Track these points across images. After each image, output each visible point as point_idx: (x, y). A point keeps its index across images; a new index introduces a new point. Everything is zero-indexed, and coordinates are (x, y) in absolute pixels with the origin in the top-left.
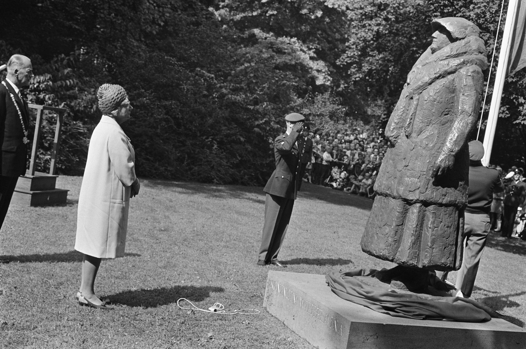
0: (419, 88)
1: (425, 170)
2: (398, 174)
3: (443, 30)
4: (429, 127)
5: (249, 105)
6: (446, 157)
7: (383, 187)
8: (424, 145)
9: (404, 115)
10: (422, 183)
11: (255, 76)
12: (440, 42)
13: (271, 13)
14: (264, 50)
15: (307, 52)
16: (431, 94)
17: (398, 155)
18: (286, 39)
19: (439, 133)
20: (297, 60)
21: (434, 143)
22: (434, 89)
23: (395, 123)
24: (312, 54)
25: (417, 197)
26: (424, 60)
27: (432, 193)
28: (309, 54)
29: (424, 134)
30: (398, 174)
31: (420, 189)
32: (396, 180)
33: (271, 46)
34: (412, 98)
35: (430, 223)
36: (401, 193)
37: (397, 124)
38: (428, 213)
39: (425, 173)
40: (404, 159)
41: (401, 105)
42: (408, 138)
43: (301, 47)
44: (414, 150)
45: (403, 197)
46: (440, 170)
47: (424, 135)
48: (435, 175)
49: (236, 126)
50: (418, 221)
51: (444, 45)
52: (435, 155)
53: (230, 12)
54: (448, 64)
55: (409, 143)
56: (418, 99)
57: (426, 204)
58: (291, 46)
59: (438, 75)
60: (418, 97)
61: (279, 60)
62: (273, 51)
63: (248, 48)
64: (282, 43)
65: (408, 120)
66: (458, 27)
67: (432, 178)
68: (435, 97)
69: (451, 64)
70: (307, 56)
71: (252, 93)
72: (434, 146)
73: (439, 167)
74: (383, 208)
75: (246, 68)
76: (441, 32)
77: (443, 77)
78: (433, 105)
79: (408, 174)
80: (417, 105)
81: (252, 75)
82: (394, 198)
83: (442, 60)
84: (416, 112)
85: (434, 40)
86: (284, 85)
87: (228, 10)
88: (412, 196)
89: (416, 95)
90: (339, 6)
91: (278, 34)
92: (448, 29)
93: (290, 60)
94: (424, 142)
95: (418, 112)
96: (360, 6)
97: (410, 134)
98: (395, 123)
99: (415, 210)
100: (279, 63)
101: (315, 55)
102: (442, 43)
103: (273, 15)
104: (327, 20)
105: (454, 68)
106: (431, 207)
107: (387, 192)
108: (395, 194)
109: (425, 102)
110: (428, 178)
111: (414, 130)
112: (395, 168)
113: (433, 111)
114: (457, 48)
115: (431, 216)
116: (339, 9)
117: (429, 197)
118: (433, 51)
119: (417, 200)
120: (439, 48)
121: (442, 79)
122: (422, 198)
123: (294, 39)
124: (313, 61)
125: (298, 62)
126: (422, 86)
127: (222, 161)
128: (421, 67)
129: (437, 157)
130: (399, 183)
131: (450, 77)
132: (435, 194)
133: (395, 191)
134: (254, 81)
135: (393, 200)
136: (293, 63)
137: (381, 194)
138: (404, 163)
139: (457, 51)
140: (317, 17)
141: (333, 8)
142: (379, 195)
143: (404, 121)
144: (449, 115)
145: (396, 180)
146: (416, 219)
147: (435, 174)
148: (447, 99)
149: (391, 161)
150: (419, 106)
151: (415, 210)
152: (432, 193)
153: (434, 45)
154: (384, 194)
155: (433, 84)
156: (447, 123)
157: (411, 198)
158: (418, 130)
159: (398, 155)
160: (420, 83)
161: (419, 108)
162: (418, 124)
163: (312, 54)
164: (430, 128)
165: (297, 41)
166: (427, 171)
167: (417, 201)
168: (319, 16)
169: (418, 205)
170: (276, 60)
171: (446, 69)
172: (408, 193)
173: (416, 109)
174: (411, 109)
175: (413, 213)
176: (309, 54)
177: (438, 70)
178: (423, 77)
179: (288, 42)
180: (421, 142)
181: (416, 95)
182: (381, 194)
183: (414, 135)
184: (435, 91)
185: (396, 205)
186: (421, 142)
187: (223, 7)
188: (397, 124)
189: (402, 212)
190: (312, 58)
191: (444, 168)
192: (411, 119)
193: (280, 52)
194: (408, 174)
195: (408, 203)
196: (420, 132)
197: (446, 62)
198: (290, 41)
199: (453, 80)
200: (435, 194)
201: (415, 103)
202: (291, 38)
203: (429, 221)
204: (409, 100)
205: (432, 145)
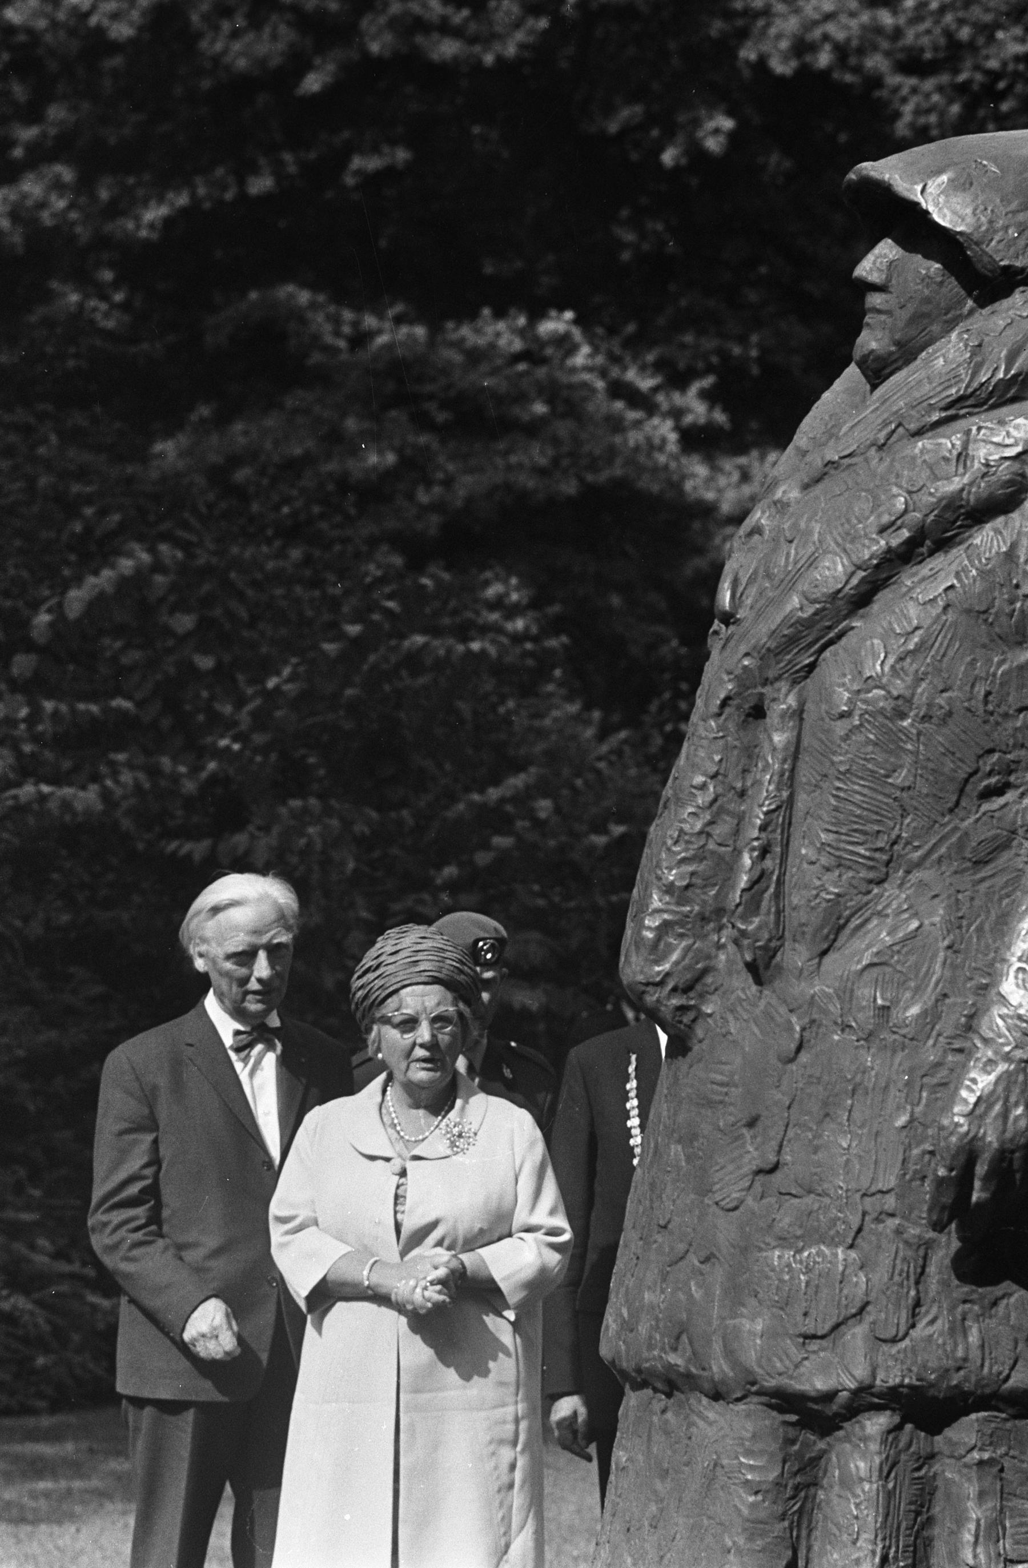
0: (792, 641)
1: (892, 1182)
2: (725, 1231)
3: (913, 227)
4: (890, 889)
5: (170, 834)
6: (1006, 1080)
7: (643, 1329)
8: (864, 1018)
9: (720, 830)
10: (880, 1275)
11: (205, 624)
12: (911, 308)
13: (373, 164)
14: (351, 424)
15: (660, 398)
16: (875, 668)
17: (710, 1104)
18: (501, 326)
19: (956, 924)
20: (593, 465)
21: (929, 995)
22: (888, 634)
23: (669, 889)
24: (696, 409)
25: (861, 1372)
26: (819, 444)
27: (958, 1329)
28: (677, 414)
29: (858, 943)
30: (725, 1231)
31: (869, 1318)
32: (718, 1274)
33: (399, 386)
34: (758, 712)
35: (968, 1537)
36: (750, 1357)
37: (679, 894)
38: (948, 1471)
39: (890, 1202)
40: (751, 1124)
41: (695, 767)
42: (759, 981)
43: (615, 372)
44: (804, 1057)
45: (771, 1383)
46: (981, 1169)
47: (860, 950)
48: (953, 1206)
49: (98, 989)
50: (888, 1530)
51: (936, 328)
52: (942, 1074)
53: (85, 184)
54: (963, 457)
55: (768, 1016)
56: (799, 714)
57: (925, 1409)
58: (541, 372)
59: (905, 534)
60: (792, 701)
61: (467, 480)
62: (422, 422)
63: (239, 427)
64: (475, 357)
65: (747, 861)
66: (1005, 200)
67: (939, 1226)
68: (899, 687)
69: (981, 453)
70: (665, 429)
71: (197, 751)
72: (931, 1016)
73: (969, 1154)
74: (664, 1474)
75: (139, 579)
76: (907, 244)
77: (943, 545)
78: (891, 742)
79: (785, 1221)
80: (795, 752)
81: (185, 622)
82: (716, 1396)
83: (919, 433)
84: (791, 800)
85: (875, 300)
86: (414, 661)
87: (67, 174)
88: (825, 1369)
89: (783, 686)
90: (842, 51)
91: (447, 299)
92: (942, 218)
93: (542, 472)
94: (864, 992)
95: (802, 801)
96: (949, 34)
97: (770, 953)
98: (669, 889)
99: (859, 1458)
100: (469, 500)
101: (720, 417)
102: (916, 318)
103: (388, 173)
104: (775, 161)
105: (1004, 472)
106: (966, 1431)
107: (673, 1358)
108: (719, 1367)
109: (840, 728)
110: (913, 1231)
111: (793, 919)
112: (704, 1190)
113: (900, 778)
114: (1012, 337)
115: (972, 1489)
116: (849, 78)
117: (934, 1359)
118: (877, 372)
119: (863, 1390)
120: (906, 352)
121: (938, 561)
122: (891, 1376)
123: (556, 324)
124: (709, 459)
125: (603, 477)
126: (808, 624)
127: (20, 1247)
128: (795, 494)
129: (947, 1087)
130: (737, 1294)
131: (988, 539)
132: (974, 1338)
133: (717, 1347)
134: (205, 662)
135: (713, 1411)
136: (569, 488)
137: (642, 1381)
138: (753, 1153)
139: (1010, 360)
140: (696, 153)
141: (805, 72)
142: (637, 1386)
143: (728, 866)
144: (1010, 796)
145: (718, 1274)
146: (871, 1518)
147: (947, 1199)
148: (980, 690)
149: (676, 1150)
150: (805, 758)
151: (859, 1458)
152: (958, 1329)
153: (871, 341)
154: (652, 1372)
155: (883, 597)
156: (1006, 845)
157: (820, 1384)
158: (815, 919)
159: (710, 1104)
160: (795, 601)
161: (805, 774)
162: (813, 878)
163: (696, 409)
164: (893, 895)
165: (577, 333)
166: (903, 1190)
167: (864, 1400)
168: (713, 144)
169: (876, 1424)
170: (448, 483)
171: (955, 484)
172: (796, 1354)
173: (789, 780)
174: (757, 783)
175: (848, 1482)
176: (677, 414)
177: (900, 503)
178: (812, 562)
179: (518, 345)
180: (846, 994)
181: (783, 686)
182: (642, 1381)
183: (796, 956)
184: (898, 646)
185: (735, 1442)
186: (846, 994)
187: (39, 156)
188: (679, 894)
189: (778, 1484)
190: (697, 440)
191: (1003, 1155)
192: (765, 851)
193: (479, 420)
194: (785, 1221)
195: (813, 1418)
196: (833, 930)
197: (949, 442)
198: (526, 332)
199: (1010, 555)
200: (974, 1338)
201: (778, 738)
202: (537, 315)
203: (960, 1521)
204: (744, 725)
205: (914, 1010)
